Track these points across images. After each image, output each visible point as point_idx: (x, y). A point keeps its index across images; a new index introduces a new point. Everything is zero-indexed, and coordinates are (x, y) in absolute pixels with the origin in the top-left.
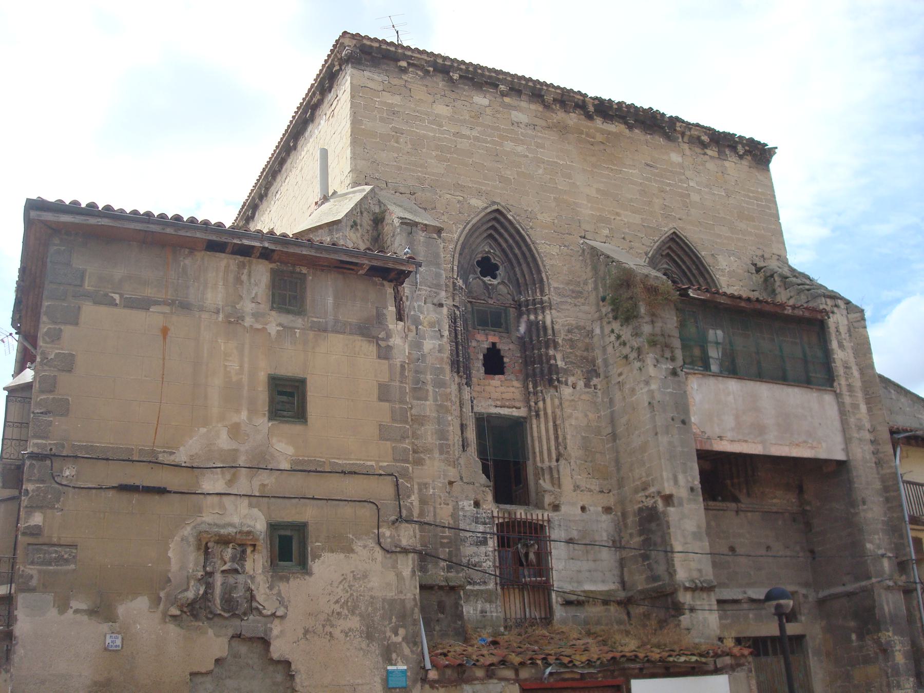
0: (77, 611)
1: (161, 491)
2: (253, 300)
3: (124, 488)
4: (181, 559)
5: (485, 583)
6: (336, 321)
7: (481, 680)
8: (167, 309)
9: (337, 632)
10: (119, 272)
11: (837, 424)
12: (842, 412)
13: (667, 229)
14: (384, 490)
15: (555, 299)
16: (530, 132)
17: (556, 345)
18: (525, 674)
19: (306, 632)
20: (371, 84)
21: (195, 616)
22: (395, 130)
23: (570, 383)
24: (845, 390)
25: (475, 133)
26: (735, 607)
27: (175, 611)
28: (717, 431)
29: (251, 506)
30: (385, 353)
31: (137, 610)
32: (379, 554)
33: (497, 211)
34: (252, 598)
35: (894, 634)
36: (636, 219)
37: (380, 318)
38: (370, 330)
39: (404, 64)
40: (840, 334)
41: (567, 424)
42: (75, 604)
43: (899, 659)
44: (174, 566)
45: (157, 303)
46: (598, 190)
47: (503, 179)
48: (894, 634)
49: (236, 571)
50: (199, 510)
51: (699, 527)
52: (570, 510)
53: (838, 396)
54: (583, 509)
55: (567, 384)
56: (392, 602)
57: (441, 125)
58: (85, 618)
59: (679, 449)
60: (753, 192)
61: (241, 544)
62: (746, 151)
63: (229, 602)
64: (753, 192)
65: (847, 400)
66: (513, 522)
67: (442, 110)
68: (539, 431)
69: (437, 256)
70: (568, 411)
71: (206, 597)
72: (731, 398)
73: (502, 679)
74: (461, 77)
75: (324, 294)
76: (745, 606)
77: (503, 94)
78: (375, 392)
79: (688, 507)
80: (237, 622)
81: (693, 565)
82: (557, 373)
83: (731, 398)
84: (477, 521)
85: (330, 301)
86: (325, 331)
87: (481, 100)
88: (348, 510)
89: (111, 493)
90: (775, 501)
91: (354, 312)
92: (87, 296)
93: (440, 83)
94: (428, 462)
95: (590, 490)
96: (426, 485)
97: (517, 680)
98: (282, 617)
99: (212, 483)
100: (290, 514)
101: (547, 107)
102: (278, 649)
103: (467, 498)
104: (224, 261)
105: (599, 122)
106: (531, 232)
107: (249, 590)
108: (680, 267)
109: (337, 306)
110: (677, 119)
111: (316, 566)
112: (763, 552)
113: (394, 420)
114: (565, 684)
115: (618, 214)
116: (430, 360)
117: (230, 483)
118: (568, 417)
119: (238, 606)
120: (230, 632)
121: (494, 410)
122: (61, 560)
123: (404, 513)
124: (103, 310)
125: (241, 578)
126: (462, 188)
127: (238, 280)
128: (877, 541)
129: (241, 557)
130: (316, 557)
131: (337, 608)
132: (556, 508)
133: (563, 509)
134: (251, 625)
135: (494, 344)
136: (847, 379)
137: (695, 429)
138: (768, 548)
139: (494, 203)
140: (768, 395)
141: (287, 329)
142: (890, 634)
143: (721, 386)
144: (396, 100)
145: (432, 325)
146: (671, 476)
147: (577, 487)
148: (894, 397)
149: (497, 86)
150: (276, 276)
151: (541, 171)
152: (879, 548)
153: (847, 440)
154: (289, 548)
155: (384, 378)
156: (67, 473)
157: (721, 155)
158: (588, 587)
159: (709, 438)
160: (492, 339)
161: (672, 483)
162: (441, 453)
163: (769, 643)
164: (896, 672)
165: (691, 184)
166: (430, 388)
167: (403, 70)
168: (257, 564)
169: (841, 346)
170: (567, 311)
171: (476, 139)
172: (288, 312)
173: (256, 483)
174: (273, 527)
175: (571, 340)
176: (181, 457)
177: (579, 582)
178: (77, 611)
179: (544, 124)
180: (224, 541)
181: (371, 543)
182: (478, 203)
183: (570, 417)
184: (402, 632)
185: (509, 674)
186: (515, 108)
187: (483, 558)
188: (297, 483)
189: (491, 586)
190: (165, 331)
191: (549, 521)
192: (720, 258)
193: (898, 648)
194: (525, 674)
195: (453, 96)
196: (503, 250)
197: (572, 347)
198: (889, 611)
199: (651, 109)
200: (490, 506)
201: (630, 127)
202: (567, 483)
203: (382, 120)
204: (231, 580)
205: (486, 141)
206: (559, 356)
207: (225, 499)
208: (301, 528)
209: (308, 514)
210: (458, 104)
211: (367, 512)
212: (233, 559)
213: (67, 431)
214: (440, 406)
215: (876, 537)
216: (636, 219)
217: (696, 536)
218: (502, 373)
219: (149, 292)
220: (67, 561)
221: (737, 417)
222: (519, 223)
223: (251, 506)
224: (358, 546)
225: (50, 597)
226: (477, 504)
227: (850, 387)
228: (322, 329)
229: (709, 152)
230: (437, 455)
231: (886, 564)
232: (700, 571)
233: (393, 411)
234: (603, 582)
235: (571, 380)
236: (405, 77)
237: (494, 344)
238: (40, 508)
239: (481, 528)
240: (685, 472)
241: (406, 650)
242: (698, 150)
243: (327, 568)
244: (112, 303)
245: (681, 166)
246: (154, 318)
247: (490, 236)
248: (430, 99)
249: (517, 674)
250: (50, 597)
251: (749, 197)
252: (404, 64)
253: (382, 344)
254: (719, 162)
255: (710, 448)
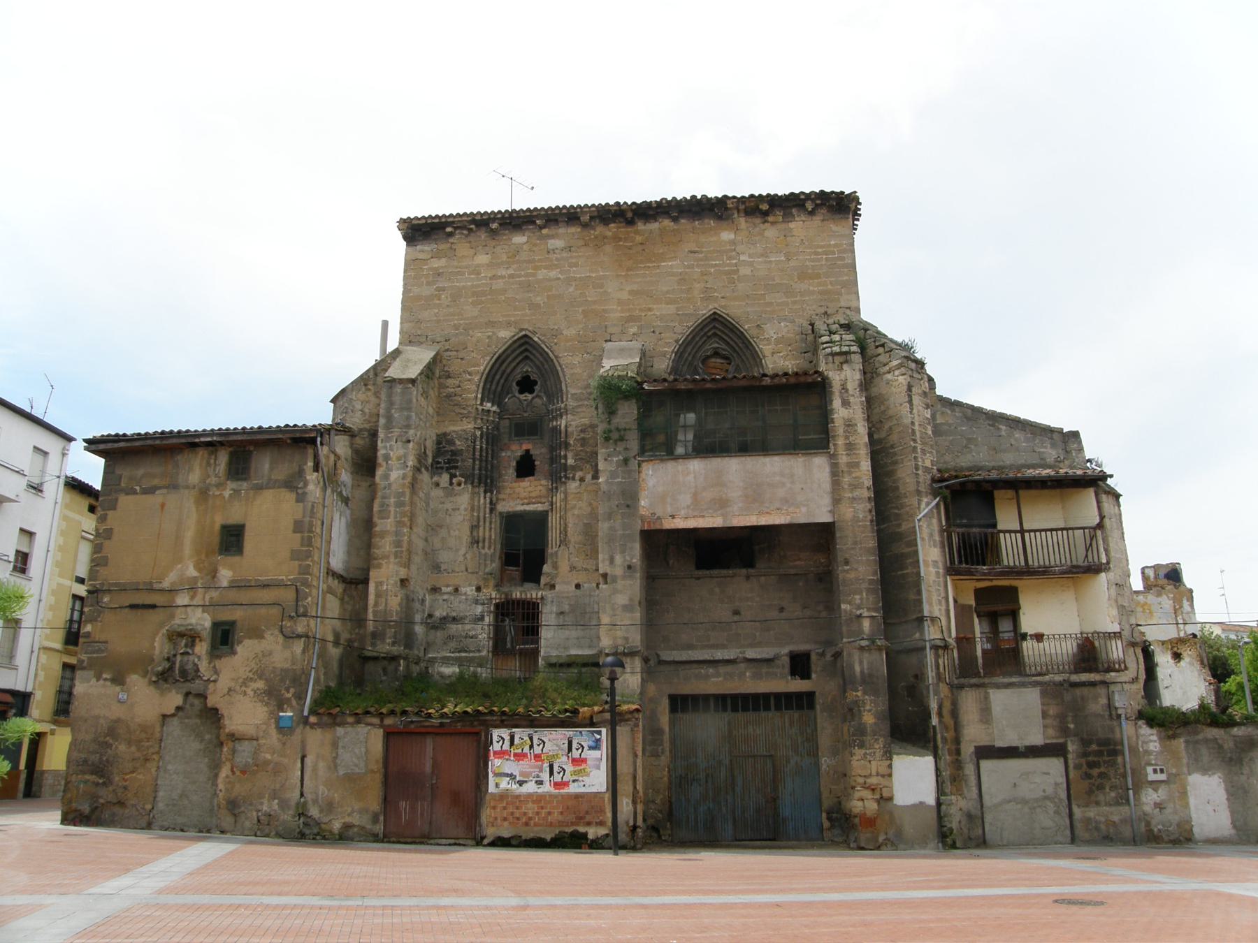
0: (106, 679)
1: (153, 607)
2: (216, 476)
3: (133, 607)
4: (160, 647)
5: (479, 651)
6: (270, 480)
7: (352, 724)
8: (164, 491)
9: (249, 692)
10: (140, 472)
11: (827, 485)
12: (835, 473)
13: (705, 312)
14: (288, 596)
15: (571, 403)
16: (565, 255)
17: (567, 445)
18: (389, 721)
19: (230, 690)
20: (421, 256)
21: (166, 680)
22: (438, 289)
23: (577, 477)
24: (841, 451)
25: (511, 271)
26: (729, 668)
27: (154, 679)
28: (669, 510)
29: (203, 611)
30: (301, 498)
31: (135, 680)
32: (281, 639)
33: (525, 336)
34: (198, 670)
35: (865, 693)
36: (671, 309)
37: (300, 473)
38: (293, 483)
39: (449, 229)
40: (847, 391)
41: (569, 515)
42: (105, 676)
43: (869, 719)
44: (157, 652)
45: (160, 488)
46: (631, 292)
47: (534, 307)
48: (865, 693)
49: (187, 653)
50: (172, 616)
51: (631, 600)
52: (565, 587)
53: (832, 457)
54: (578, 586)
55: (573, 479)
56: (286, 670)
57: (479, 274)
58: (109, 683)
59: (620, 532)
60: (822, 247)
61: (191, 637)
62: (817, 205)
63: (184, 673)
64: (822, 247)
65: (843, 459)
66: (508, 602)
67: (482, 259)
68: (553, 521)
69: (410, 401)
70: (572, 502)
71: (171, 668)
72: (691, 478)
73: (368, 724)
74: (501, 225)
75: (264, 464)
76: (742, 665)
77: (541, 228)
78: (291, 527)
79: (620, 584)
80: (188, 684)
81: (619, 634)
82: (566, 470)
83: (691, 478)
84: (476, 602)
85: (267, 466)
86: (261, 488)
87: (519, 239)
88: (263, 611)
89: (127, 610)
90: (798, 563)
91: (283, 471)
92: (122, 490)
93: (483, 235)
94: (385, 566)
95: (586, 570)
96: (381, 583)
97: (381, 726)
98: (215, 681)
99: (182, 599)
100: (226, 616)
101: (585, 226)
102: (212, 701)
103: (470, 585)
104: (202, 453)
105: (640, 226)
106: (555, 348)
107: (195, 665)
108: (728, 343)
109: (271, 469)
110: (725, 197)
111: (239, 649)
112: (774, 614)
113: (302, 545)
114: (423, 730)
115: (650, 310)
116: (394, 487)
117: (192, 598)
118: (572, 507)
119: (189, 675)
120: (184, 691)
121: (520, 508)
122: (100, 651)
123: (301, 610)
124: (130, 497)
125: (191, 658)
126: (491, 324)
127: (208, 464)
128: (858, 601)
129: (192, 644)
130: (240, 642)
131: (251, 675)
132: (553, 587)
133: (557, 587)
134: (196, 686)
135: (528, 451)
136: (847, 438)
137: (642, 512)
138: (782, 609)
139: (522, 330)
140: (734, 468)
141: (237, 492)
142: (859, 694)
143: (680, 468)
144: (443, 262)
145: (399, 459)
146: (607, 557)
147: (573, 568)
148: (1003, 433)
149: (534, 222)
150: (232, 455)
151: (571, 289)
152: (859, 608)
153: (836, 501)
154: (224, 637)
155: (299, 516)
156: (106, 600)
157: (788, 217)
158: (573, 652)
159: (659, 518)
160: (525, 447)
161: (607, 563)
162: (396, 557)
163: (729, 701)
164: (861, 731)
165: (742, 258)
166: (392, 509)
167: (451, 235)
168: (202, 648)
169: (846, 403)
170: (577, 417)
171: (511, 276)
172: (238, 480)
173: (207, 598)
174: (216, 625)
175: (583, 439)
176: (166, 584)
177: (566, 648)
178: (106, 679)
179: (581, 243)
180: (181, 635)
181: (277, 632)
182: (506, 334)
183: (574, 507)
184: (292, 690)
185: (376, 721)
186: (552, 237)
187: (480, 631)
188: (233, 595)
189: (484, 653)
190: (163, 506)
191: (542, 598)
192: (767, 327)
193: (868, 707)
194: (389, 721)
195: (493, 243)
196: (538, 368)
197: (582, 445)
198: (862, 672)
199: (694, 197)
200: (491, 593)
201: (675, 220)
202: (564, 566)
203: (428, 284)
204: (186, 658)
205: (520, 276)
206: (570, 455)
207: (189, 609)
208: (232, 624)
209: (237, 615)
210: (498, 250)
211: (275, 611)
212: (186, 646)
213: (110, 575)
214: (399, 522)
215: (857, 597)
216: (671, 309)
217: (628, 608)
218: (533, 475)
219: (156, 482)
220: (103, 651)
221: (695, 495)
222: (543, 342)
223: (203, 611)
224: (267, 635)
225: (92, 673)
226: (478, 589)
227: (850, 447)
228: (259, 488)
229: (770, 219)
230: (392, 560)
231: (866, 624)
232: (626, 639)
233: (303, 538)
234: (590, 647)
235: (579, 474)
236: (451, 240)
237: (528, 451)
238: (90, 621)
239: (479, 609)
240: (623, 552)
241: (294, 702)
242: (758, 221)
243: (246, 649)
244: (135, 493)
245: (733, 242)
246: (158, 498)
247: (715, 335)
248: (472, 252)
249: (382, 721)
250: (92, 673)
251: (816, 253)
252: (449, 229)
253: (300, 491)
254: (783, 226)
255: (658, 527)
